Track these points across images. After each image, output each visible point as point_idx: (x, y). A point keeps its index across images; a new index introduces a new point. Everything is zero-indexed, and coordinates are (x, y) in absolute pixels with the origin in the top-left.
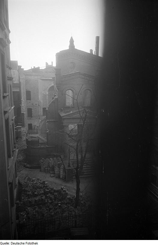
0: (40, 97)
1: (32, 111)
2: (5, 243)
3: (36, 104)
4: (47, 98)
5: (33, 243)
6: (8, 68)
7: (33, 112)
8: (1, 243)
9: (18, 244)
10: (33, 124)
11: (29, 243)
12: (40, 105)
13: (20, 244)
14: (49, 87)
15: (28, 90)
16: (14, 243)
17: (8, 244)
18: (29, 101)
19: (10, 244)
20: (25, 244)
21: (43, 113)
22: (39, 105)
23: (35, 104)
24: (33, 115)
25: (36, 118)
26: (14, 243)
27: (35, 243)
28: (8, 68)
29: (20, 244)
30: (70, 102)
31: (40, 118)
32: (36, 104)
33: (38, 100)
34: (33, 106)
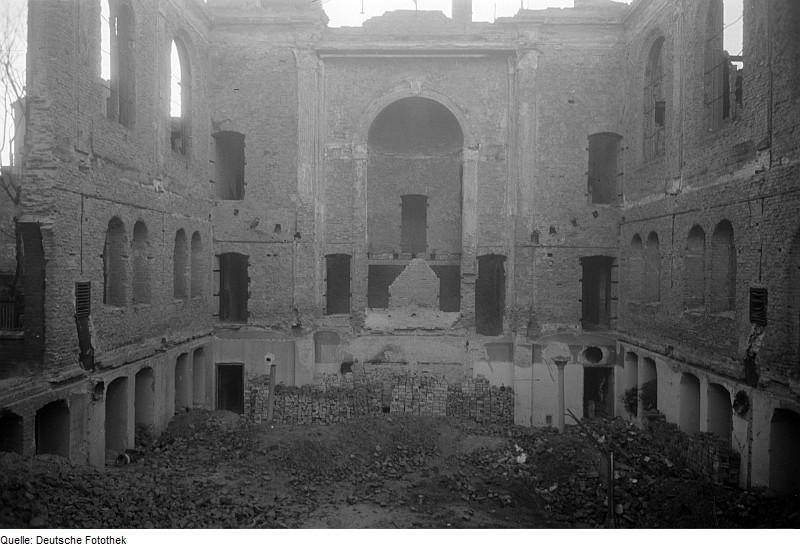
0: (304, 171)
1: (250, 272)
2: (17, 540)
3: (278, 227)
4: (358, 185)
5: (109, 540)
6: (715, 353)
7: (252, 284)
8: (4, 540)
9: (61, 541)
10: (247, 368)
11: (98, 541)
12: (303, 234)
13: (68, 541)
14: (374, 111)
15: (227, 127)
16: (46, 541)
17: (26, 541)
18: (231, 204)
19: (34, 541)
20: (84, 540)
21: (328, 295)
22: (298, 235)
23: (271, 224)
24: (251, 303)
25: (277, 328)
26: (46, 541)
27: (118, 539)
28: (715, 353)
29: (68, 541)
30: (525, 209)
31: (298, 326)
32: (278, 227)
33: (294, 198)
34: (256, 238)
